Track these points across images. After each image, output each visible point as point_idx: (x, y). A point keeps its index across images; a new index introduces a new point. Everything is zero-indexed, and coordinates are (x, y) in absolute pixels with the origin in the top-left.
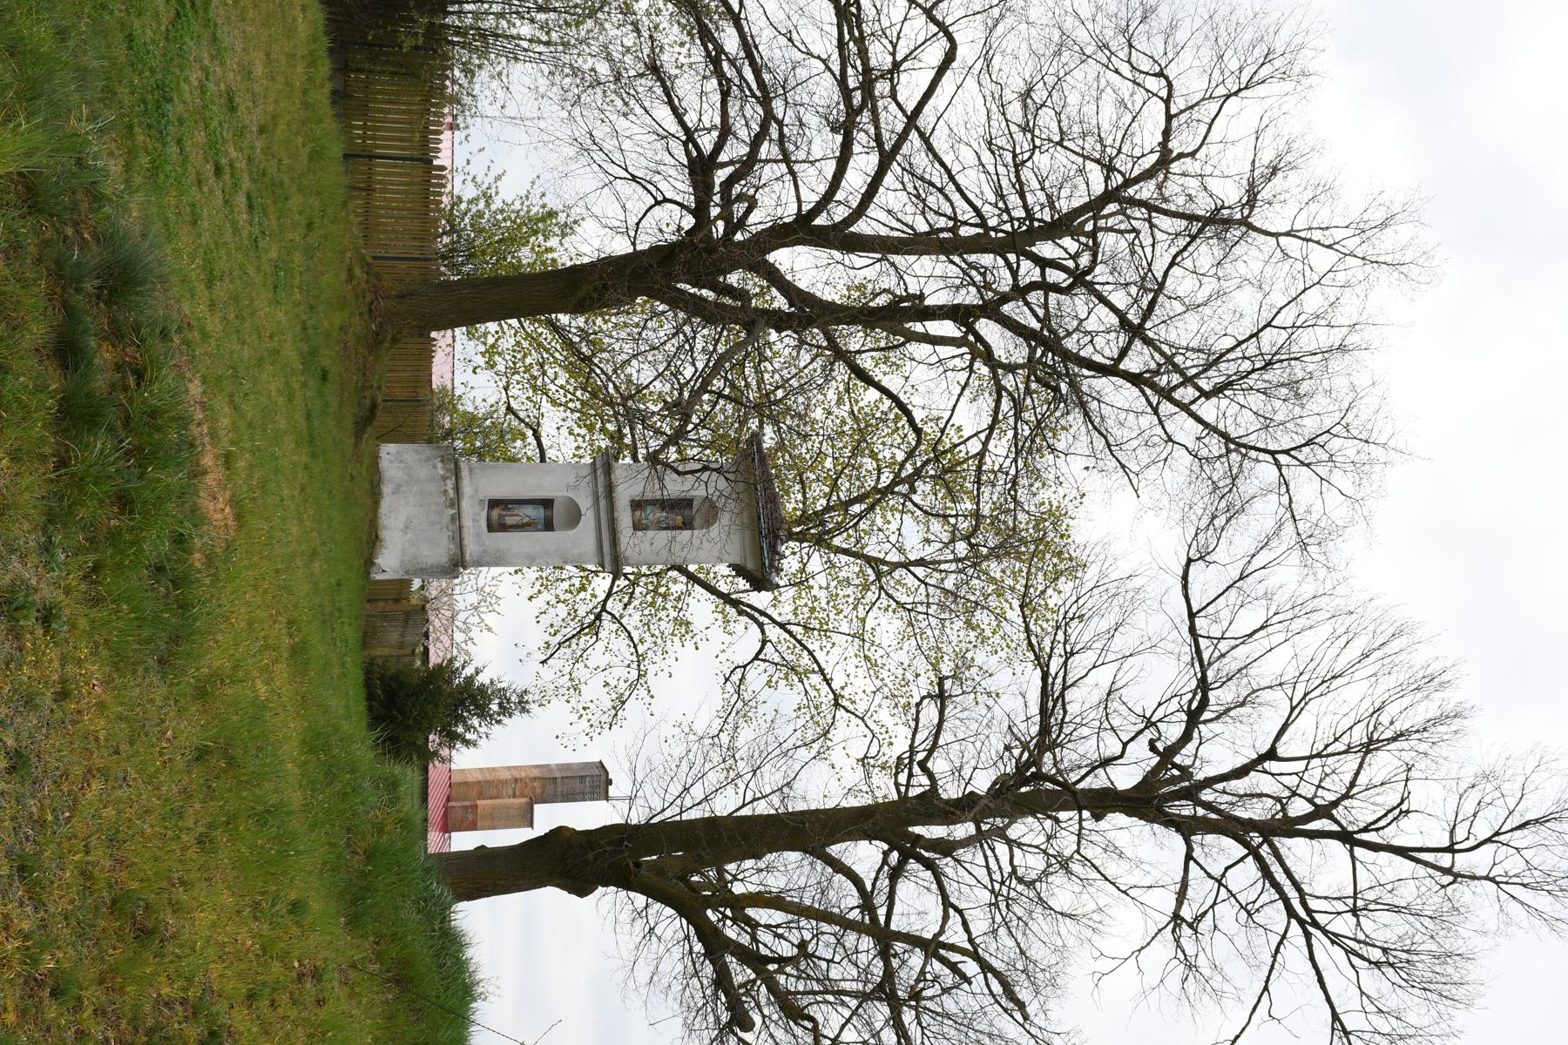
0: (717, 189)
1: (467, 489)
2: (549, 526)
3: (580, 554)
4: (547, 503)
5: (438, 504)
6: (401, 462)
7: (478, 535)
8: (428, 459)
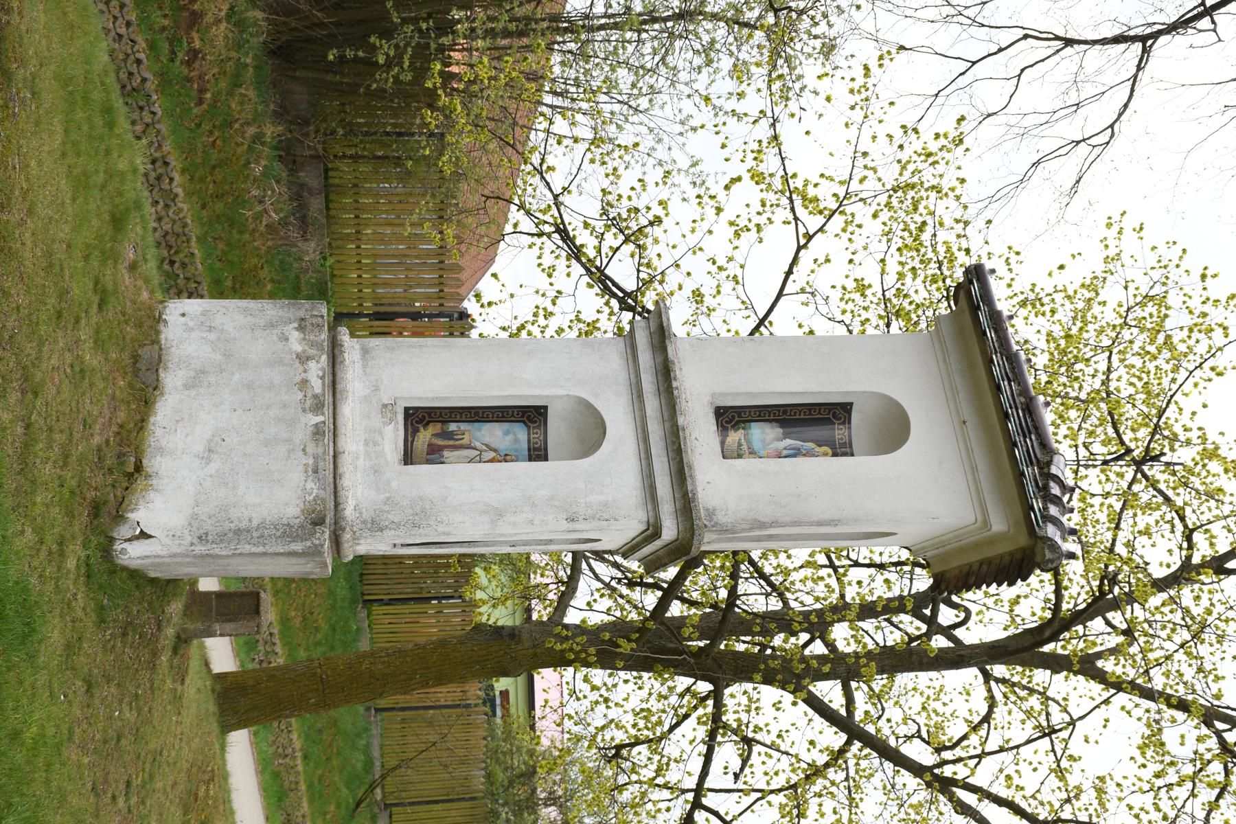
0: (308, 544)
2: (538, 453)
3: (606, 505)
4: (533, 416)
5: (285, 406)
6: (211, 329)
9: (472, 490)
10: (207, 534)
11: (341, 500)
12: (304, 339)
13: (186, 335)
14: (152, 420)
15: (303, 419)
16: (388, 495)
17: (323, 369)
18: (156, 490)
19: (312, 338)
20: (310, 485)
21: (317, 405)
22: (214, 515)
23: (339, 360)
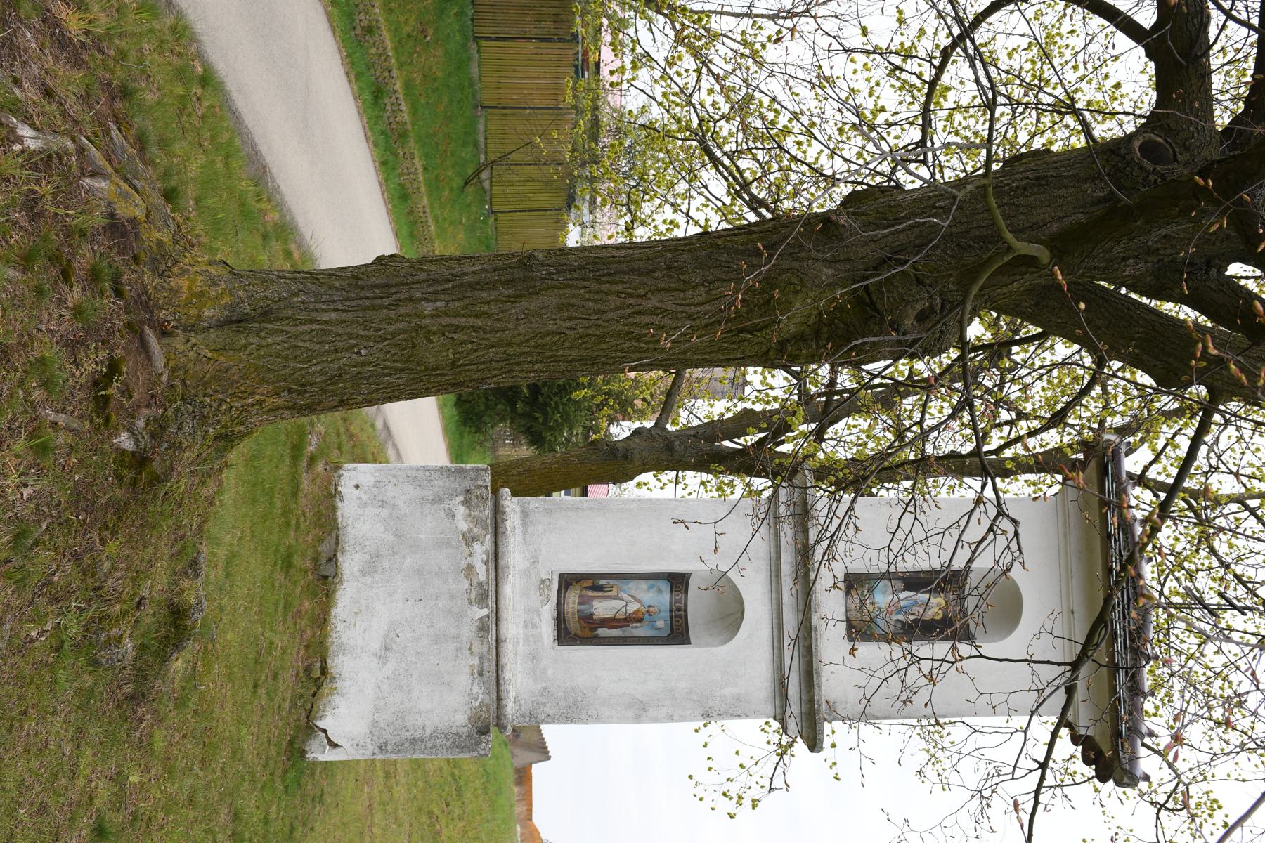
1: (515, 556)
2: (678, 633)
5: (452, 597)
6: (383, 503)
7: (534, 657)
8: (439, 499)
9: (620, 680)
10: (386, 743)
11: (503, 695)
12: (470, 515)
13: (360, 511)
14: (333, 611)
15: (469, 612)
16: (544, 685)
17: (486, 552)
18: (340, 694)
19: (477, 513)
20: (476, 689)
21: (481, 595)
22: (392, 723)
23: (501, 530)
